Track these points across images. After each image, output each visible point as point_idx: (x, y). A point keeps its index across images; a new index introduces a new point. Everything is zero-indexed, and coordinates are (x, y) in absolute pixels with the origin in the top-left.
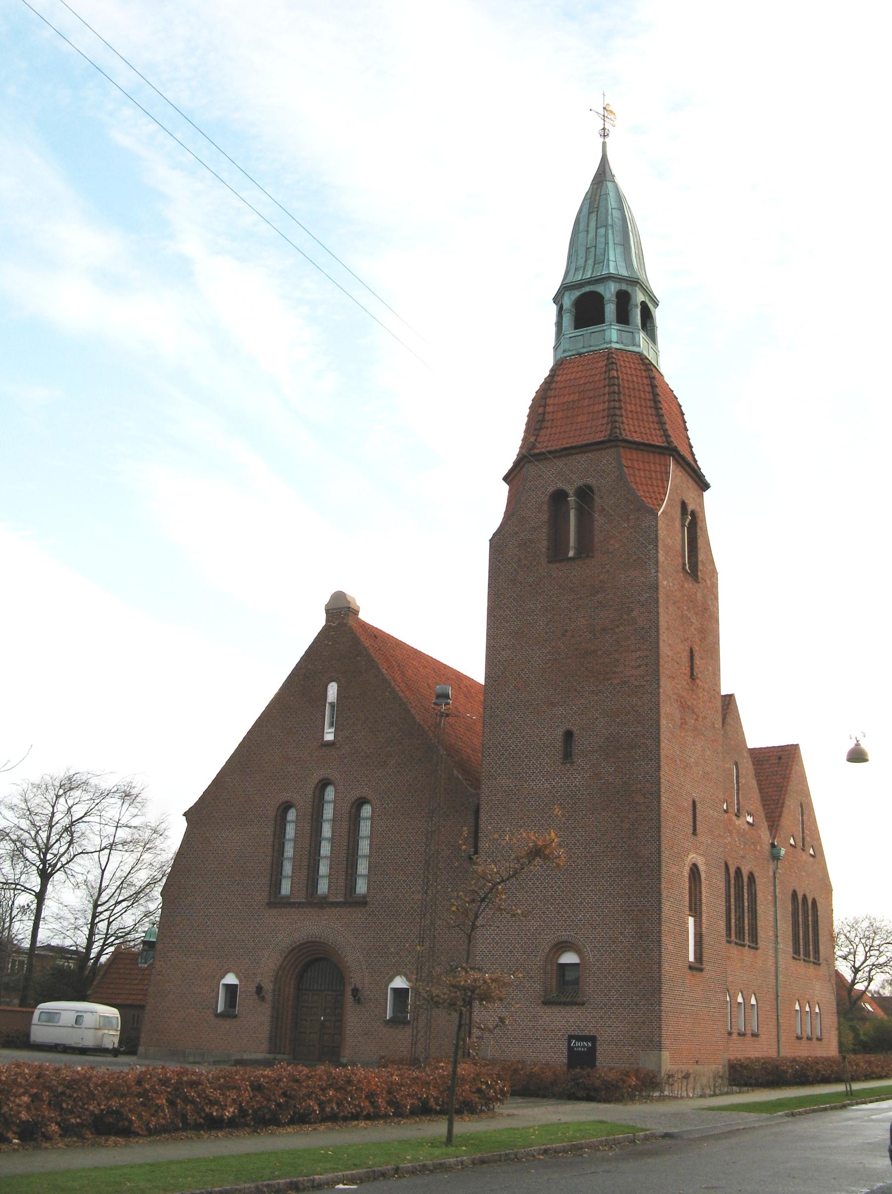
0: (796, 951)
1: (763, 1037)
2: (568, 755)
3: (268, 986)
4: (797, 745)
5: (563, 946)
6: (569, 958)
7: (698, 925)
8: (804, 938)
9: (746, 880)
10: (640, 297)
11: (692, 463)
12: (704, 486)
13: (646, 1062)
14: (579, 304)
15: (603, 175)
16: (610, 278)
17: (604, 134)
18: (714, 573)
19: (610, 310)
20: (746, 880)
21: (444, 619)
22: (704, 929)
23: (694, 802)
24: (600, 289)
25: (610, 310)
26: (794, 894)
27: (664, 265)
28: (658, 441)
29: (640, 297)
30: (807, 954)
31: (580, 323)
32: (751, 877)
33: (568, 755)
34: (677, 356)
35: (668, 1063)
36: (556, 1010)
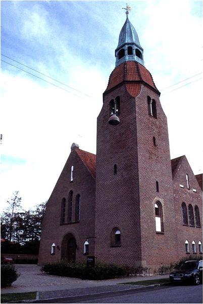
0: (186, 221)
1: (114, 251)
2: (115, 172)
3: (60, 246)
4: (184, 156)
5: (116, 229)
6: (118, 233)
7: (162, 220)
8: (190, 217)
9: (194, 208)
10: (135, 47)
11: (153, 87)
12: (158, 94)
13: (137, 264)
14: (119, 54)
15: (127, 21)
16: (126, 44)
17: (127, 13)
18: (165, 117)
19: (126, 52)
20: (194, 208)
21: (90, 146)
22: (164, 221)
23: (157, 182)
24: (123, 48)
25: (126, 52)
26: (184, 204)
27: (145, 39)
28: (138, 79)
29: (135, 47)
30: (193, 223)
31: (119, 58)
32: (196, 207)
33: (115, 172)
34: (149, 62)
35: (144, 264)
36: (114, 248)
